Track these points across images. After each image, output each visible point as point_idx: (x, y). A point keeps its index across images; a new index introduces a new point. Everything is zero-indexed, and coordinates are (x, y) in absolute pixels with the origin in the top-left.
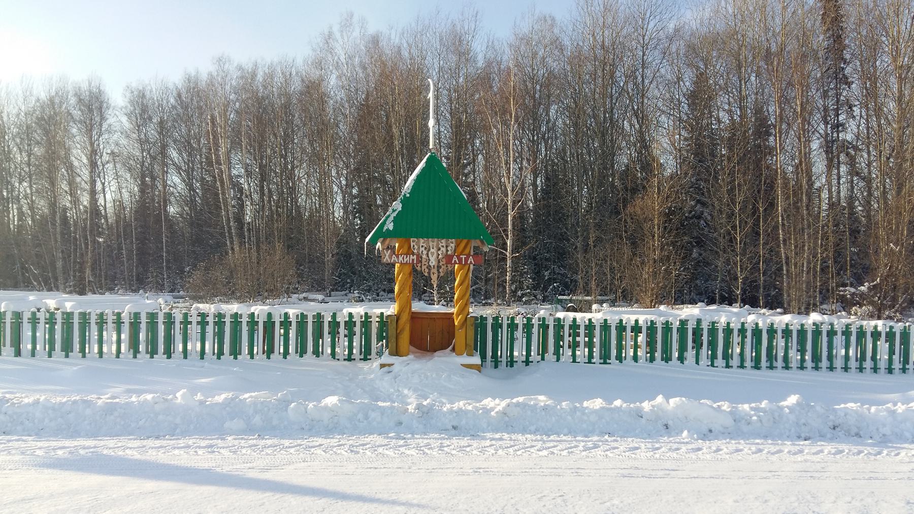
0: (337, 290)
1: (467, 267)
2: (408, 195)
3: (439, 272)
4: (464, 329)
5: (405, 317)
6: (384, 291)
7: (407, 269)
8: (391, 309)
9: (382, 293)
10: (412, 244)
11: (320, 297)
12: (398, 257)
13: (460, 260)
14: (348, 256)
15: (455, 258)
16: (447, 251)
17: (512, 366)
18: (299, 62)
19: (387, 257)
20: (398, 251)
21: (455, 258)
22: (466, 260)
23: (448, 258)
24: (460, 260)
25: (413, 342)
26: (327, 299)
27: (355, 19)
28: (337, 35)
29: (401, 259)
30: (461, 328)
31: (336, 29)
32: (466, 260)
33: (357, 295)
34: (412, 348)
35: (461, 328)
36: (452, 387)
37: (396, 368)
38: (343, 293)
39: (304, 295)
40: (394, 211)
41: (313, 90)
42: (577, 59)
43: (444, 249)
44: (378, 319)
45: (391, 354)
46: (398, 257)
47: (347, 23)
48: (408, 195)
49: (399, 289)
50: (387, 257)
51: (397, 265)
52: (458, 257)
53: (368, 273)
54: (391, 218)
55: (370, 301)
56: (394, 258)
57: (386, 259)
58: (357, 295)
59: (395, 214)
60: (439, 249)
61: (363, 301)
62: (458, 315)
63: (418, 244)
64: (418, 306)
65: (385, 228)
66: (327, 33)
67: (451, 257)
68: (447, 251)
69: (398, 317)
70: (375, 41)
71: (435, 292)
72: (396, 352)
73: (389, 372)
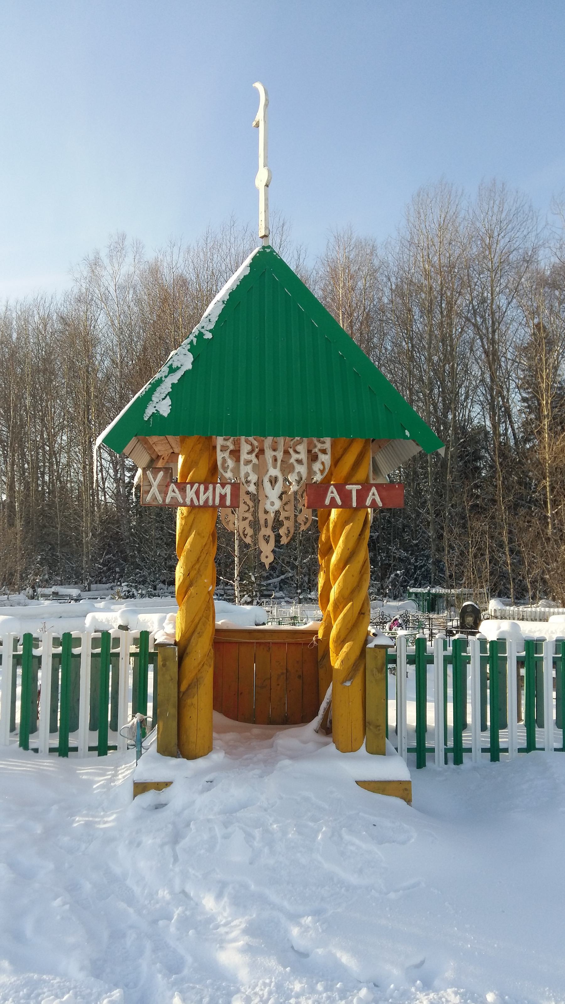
0: (101, 582)
1: (361, 517)
2: (209, 336)
3: (278, 538)
4: (358, 680)
5: (202, 648)
6: (164, 582)
7: (206, 523)
8: (163, 622)
9: (161, 585)
10: (220, 456)
11: (74, 592)
12: (182, 490)
13: (345, 496)
14: (117, 538)
15: (332, 493)
16: (311, 472)
17: (458, 761)
18: (60, 298)
19: (154, 490)
20: (184, 475)
21: (332, 493)
22: (362, 495)
23: (315, 493)
24: (345, 496)
25: (219, 704)
26: (84, 594)
27: (128, 242)
28: (106, 261)
29: (190, 493)
30: (350, 676)
31: (103, 254)
32: (362, 495)
33: (125, 588)
34: (219, 718)
35: (350, 676)
36: (354, 879)
37: (177, 796)
38: (108, 585)
39: (54, 589)
40: (172, 370)
41: (75, 337)
42: (405, 291)
43: (302, 469)
44: (134, 649)
45: (164, 750)
46: (182, 490)
47: (118, 248)
48: (209, 336)
49: (187, 575)
50: (154, 490)
51: (181, 513)
52: (340, 488)
53: (143, 559)
54: (166, 387)
55: (142, 596)
56: (173, 492)
57: (153, 495)
58: (125, 588)
59: (175, 378)
60: (291, 469)
61: (133, 596)
62: (341, 642)
63: (236, 454)
64: (239, 615)
65: (150, 411)
66: (92, 257)
67: (324, 486)
68: (311, 472)
69: (183, 649)
70: (155, 271)
71: (236, 584)
72: (178, 746)
73: (159, 807)
